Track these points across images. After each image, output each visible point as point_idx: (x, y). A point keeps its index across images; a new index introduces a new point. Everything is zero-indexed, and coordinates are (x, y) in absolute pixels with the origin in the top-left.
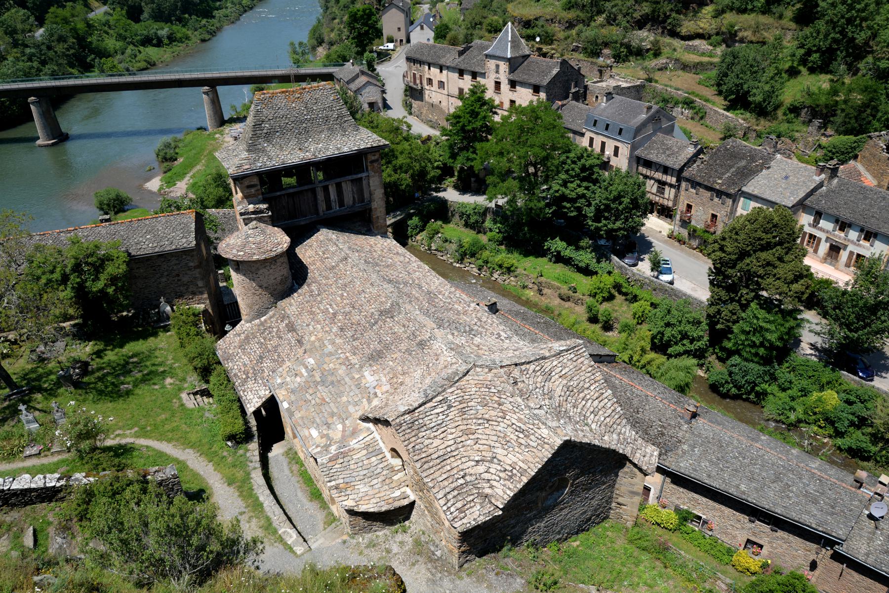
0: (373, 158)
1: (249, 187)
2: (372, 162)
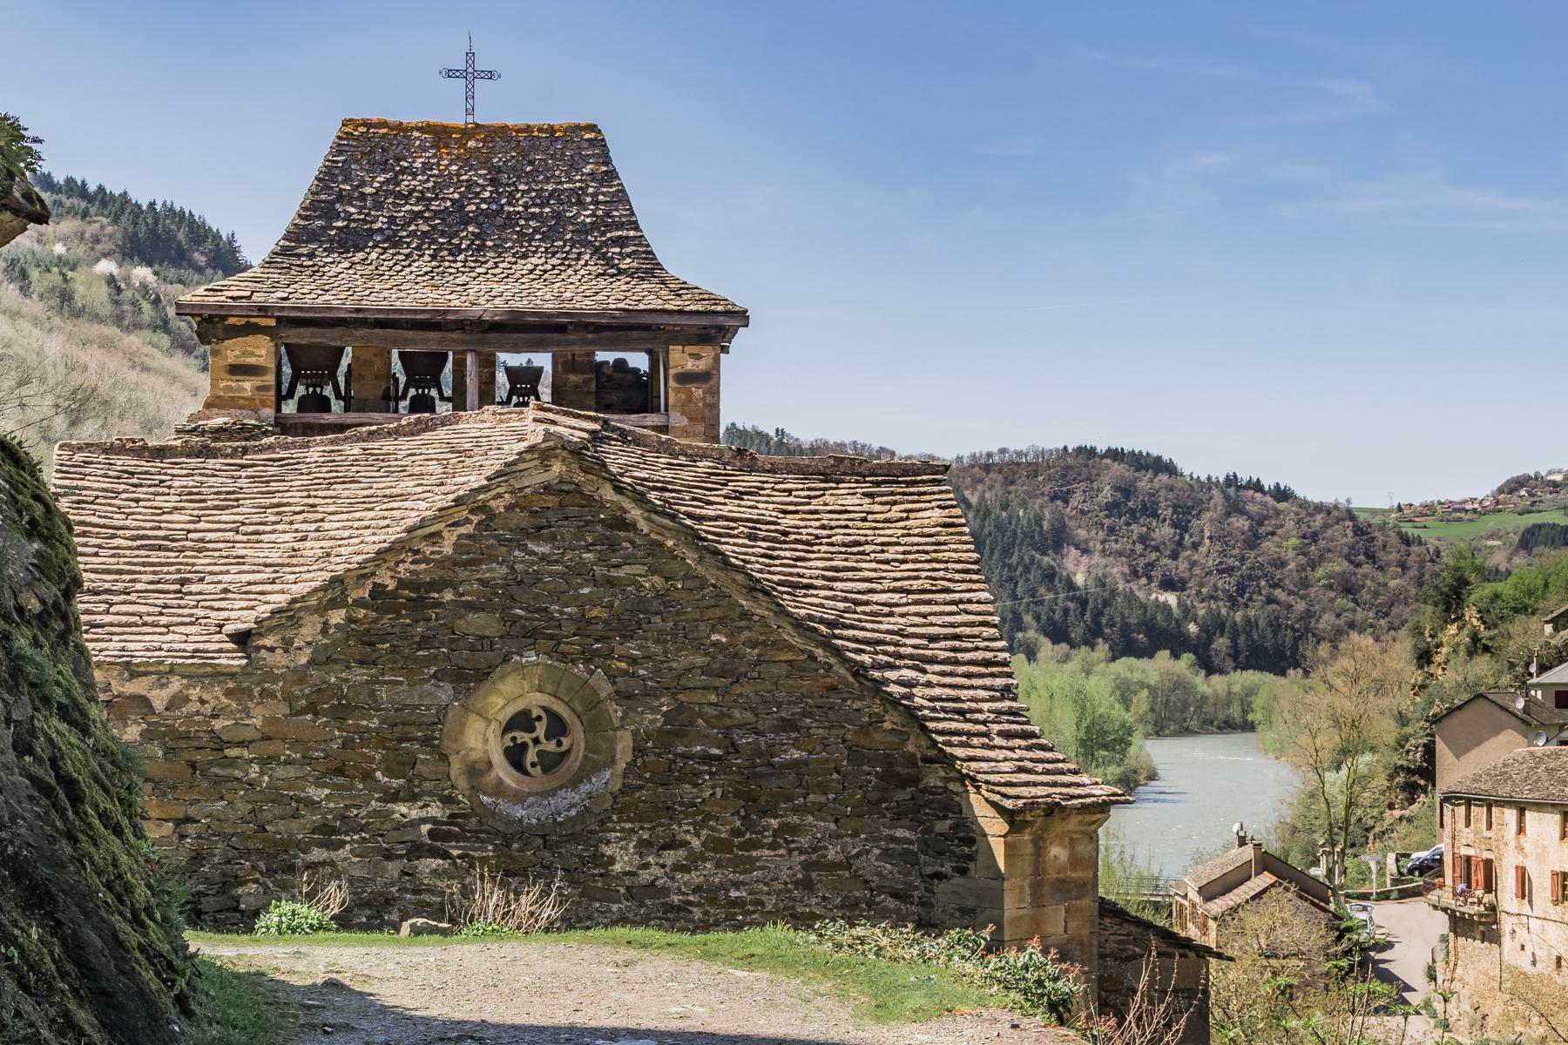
0: (691, 365)
1: (237, 370)
2: (685, 378)
